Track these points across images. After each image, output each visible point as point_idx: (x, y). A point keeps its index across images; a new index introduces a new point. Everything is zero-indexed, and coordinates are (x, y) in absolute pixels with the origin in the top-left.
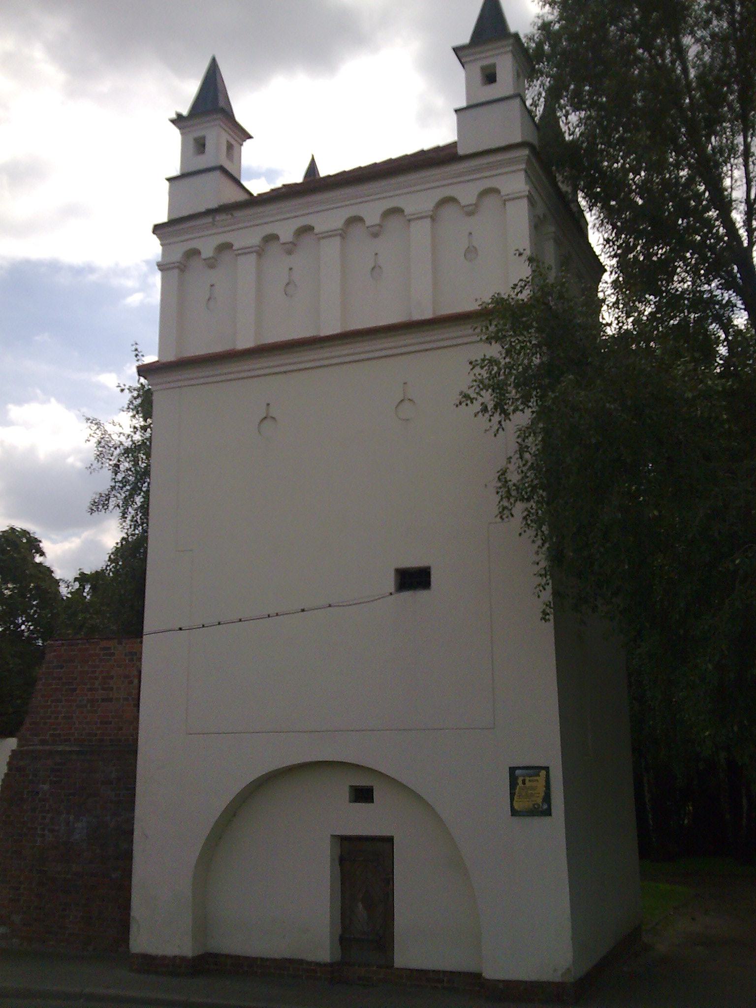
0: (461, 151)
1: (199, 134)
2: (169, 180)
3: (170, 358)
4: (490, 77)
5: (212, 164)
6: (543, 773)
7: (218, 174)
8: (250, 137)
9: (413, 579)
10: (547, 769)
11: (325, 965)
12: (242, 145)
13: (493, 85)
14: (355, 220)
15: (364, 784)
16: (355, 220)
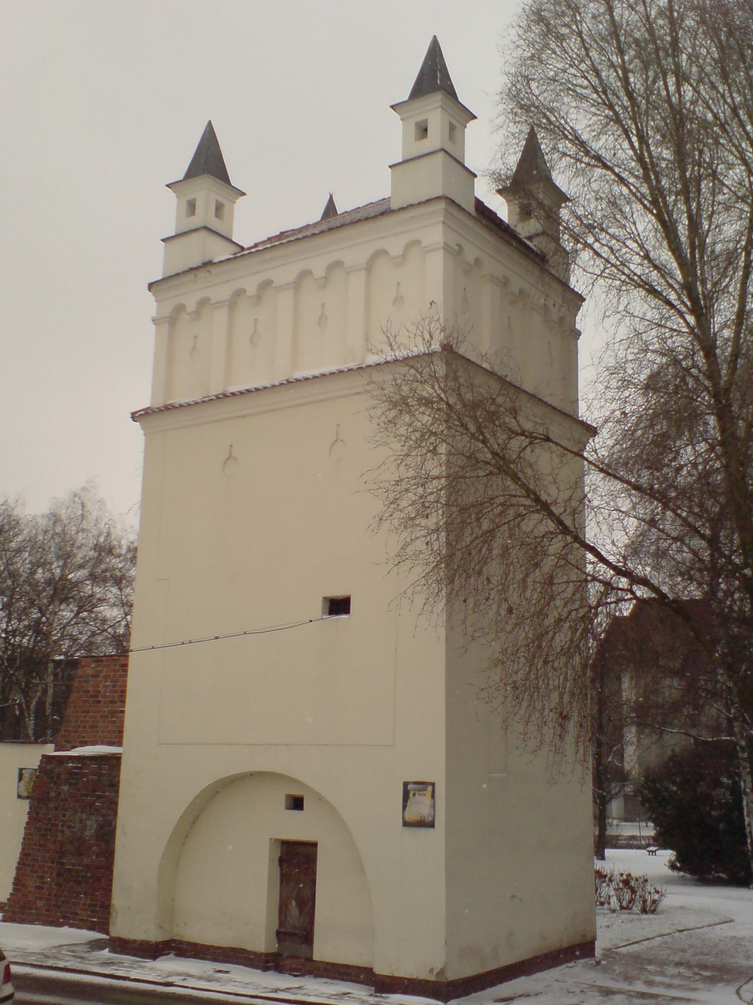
0: (394, 206)
1: (190, 197)
2: (390, 167)
3: (159, 404)
4: (423, 131)
5: (200, 225)
6: (430, 788)
7: (203, 233)
8: (475, 117)
9: (339, 606)
10: (433, 785)
11: (261, 954)
12: (465, 127)
13: (425, 140)
14: (306, 274)
15: (444, 787)
16: (240, 293)
